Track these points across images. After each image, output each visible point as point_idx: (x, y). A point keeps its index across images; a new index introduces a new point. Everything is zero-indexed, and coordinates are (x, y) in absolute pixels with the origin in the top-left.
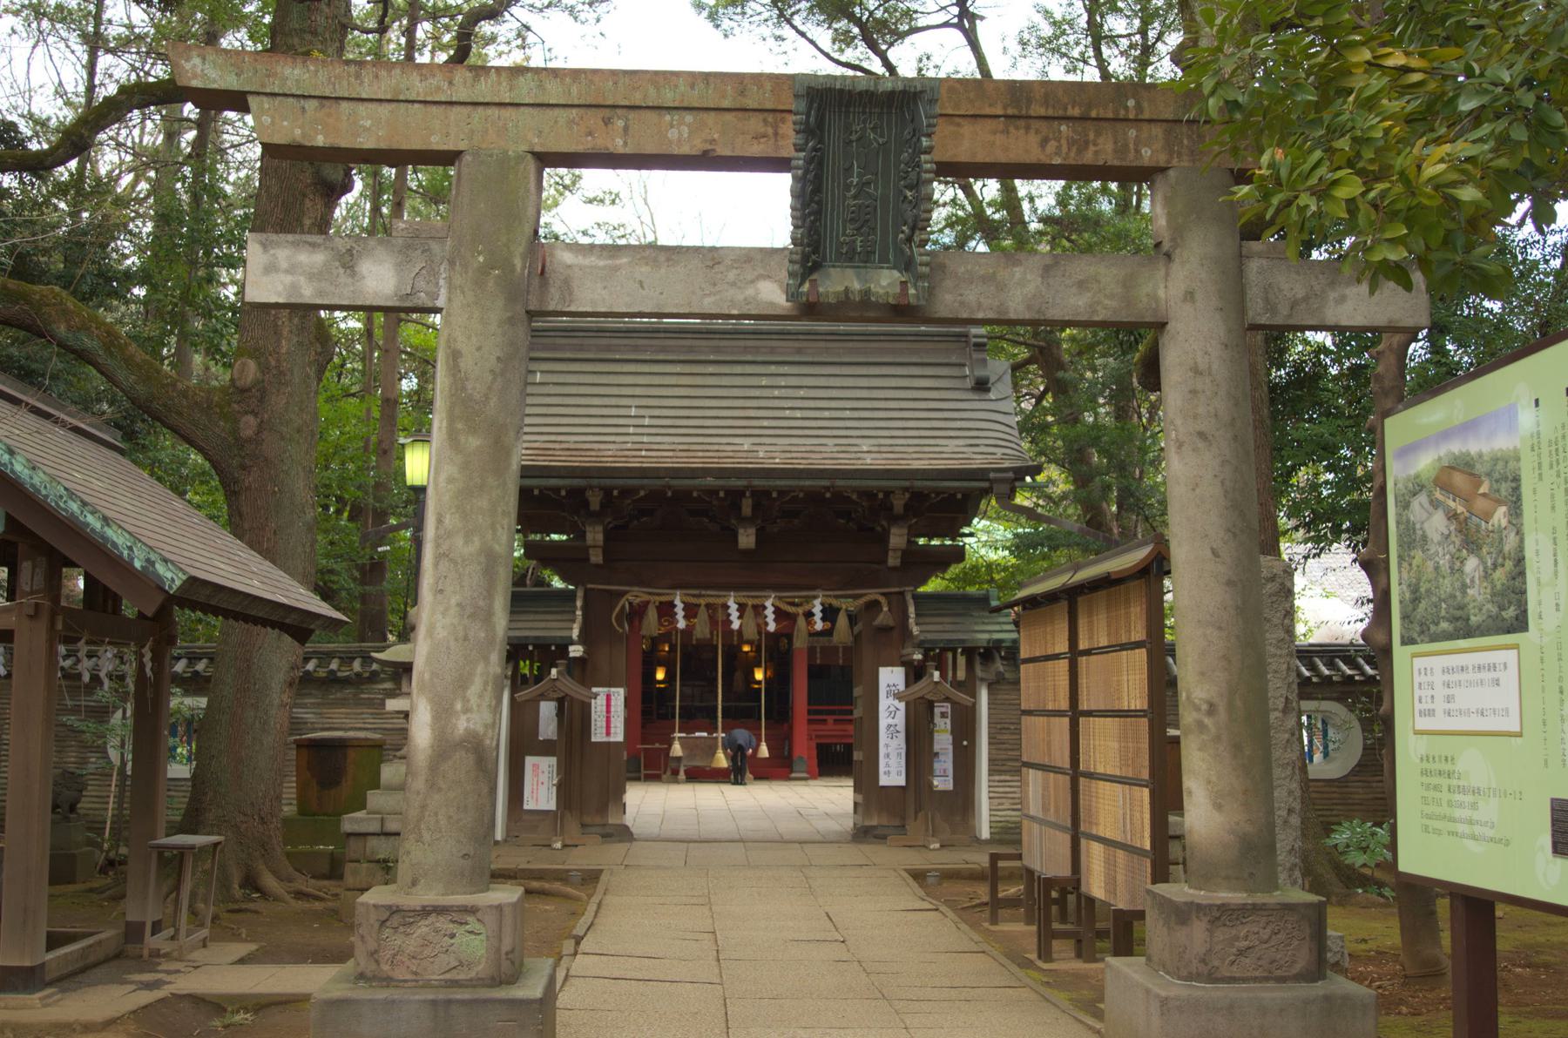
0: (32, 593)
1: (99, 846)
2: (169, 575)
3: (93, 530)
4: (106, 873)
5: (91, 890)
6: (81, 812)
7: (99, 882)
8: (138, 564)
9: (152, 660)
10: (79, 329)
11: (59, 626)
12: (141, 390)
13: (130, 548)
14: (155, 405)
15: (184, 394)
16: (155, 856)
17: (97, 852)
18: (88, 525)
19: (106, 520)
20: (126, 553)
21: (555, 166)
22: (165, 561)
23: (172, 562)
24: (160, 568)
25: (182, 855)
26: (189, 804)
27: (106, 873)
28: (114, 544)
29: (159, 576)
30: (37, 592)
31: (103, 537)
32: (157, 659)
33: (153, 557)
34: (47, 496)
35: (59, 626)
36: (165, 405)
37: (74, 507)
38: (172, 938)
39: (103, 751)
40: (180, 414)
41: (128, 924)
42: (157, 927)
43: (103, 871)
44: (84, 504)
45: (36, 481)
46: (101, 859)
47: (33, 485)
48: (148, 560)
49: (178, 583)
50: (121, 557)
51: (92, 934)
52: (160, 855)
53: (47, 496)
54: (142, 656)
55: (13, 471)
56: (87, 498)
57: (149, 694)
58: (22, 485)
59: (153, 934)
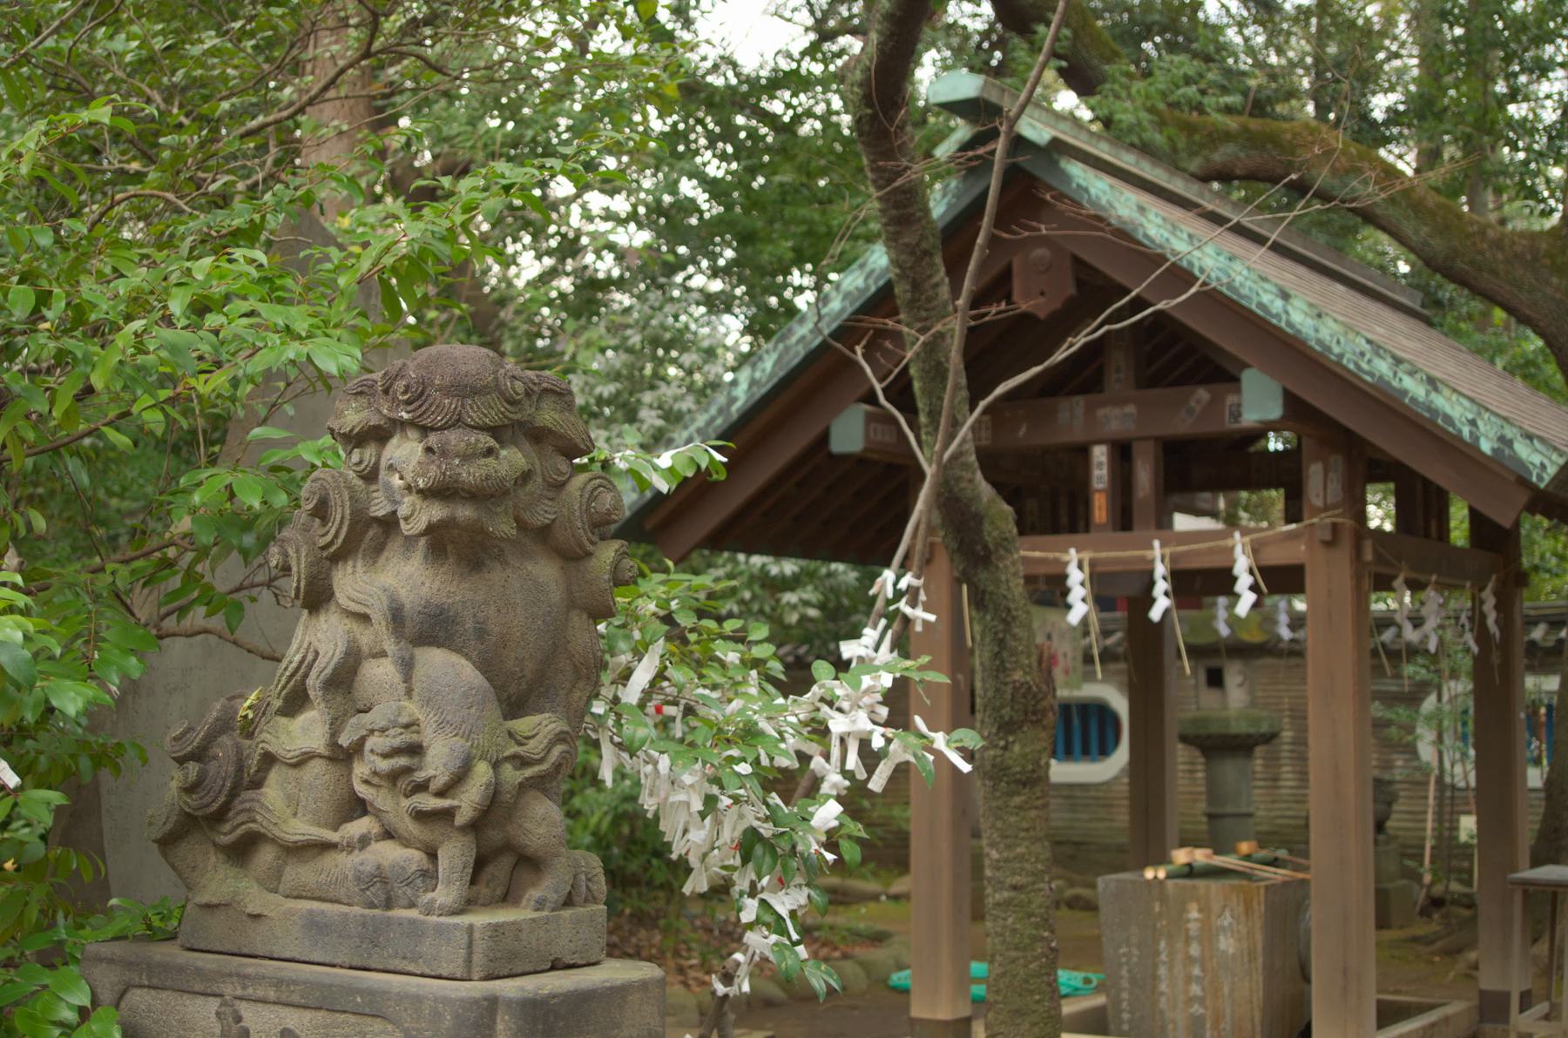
0: (1326, 508)
1: (1418, 878)
2: (1536, 459)
3: (1413, 400)
4: (1429, 916)
5: (1415, 939)
6: (1391, 832)
7: (1422, 929)
8: (1486, 446)
9: (1496, 607)
10: (1347, 172)
11: (1368, 556)
12: (1438, 245)
13: (1473, 423)
14: (1460, 264)
15: (1498, 244)
16: (1518, 897)
17: (1416, 887)
18: (1405, 392)
19: (1432, 382)
20: (1466, 431)
21: (1448, 531)
22: (1530, 437)
23: (1542, 440)
24: (1522, 449)
25: (1555, 894)
26: (1544, 821)
27: (1429, 916)
28: (1448, 419)
29: (1521, 462)
30: (1334, 507)
31: (1429, 409)
32: (1504, 606)
33: (1509, 432)
34: (1341, 356)
35: (1368, 556)
36: (1472, 263)
37: (1383, 367)
38: (1547, 1017)
39: (1411, 750)
40: (1493, 272)
41: (1483, 994)
42: (1526, 1001)
43: (1425, 912)
44: (1398, 361)
45: (1325, 334)
46: (1421, 896)
47: (1319, 341)
48: (1502, 439)
49: (1552, 470)
50: (1459, 437)
51: (1432, 1007)
52: (1525, 892)
53: (1341, 356)
54: (1482, 602)
55: (1289, 324)
56: (1399, 353)
57: (1495, 659)
58: (1303, 343)
59: (1522, 1011)
